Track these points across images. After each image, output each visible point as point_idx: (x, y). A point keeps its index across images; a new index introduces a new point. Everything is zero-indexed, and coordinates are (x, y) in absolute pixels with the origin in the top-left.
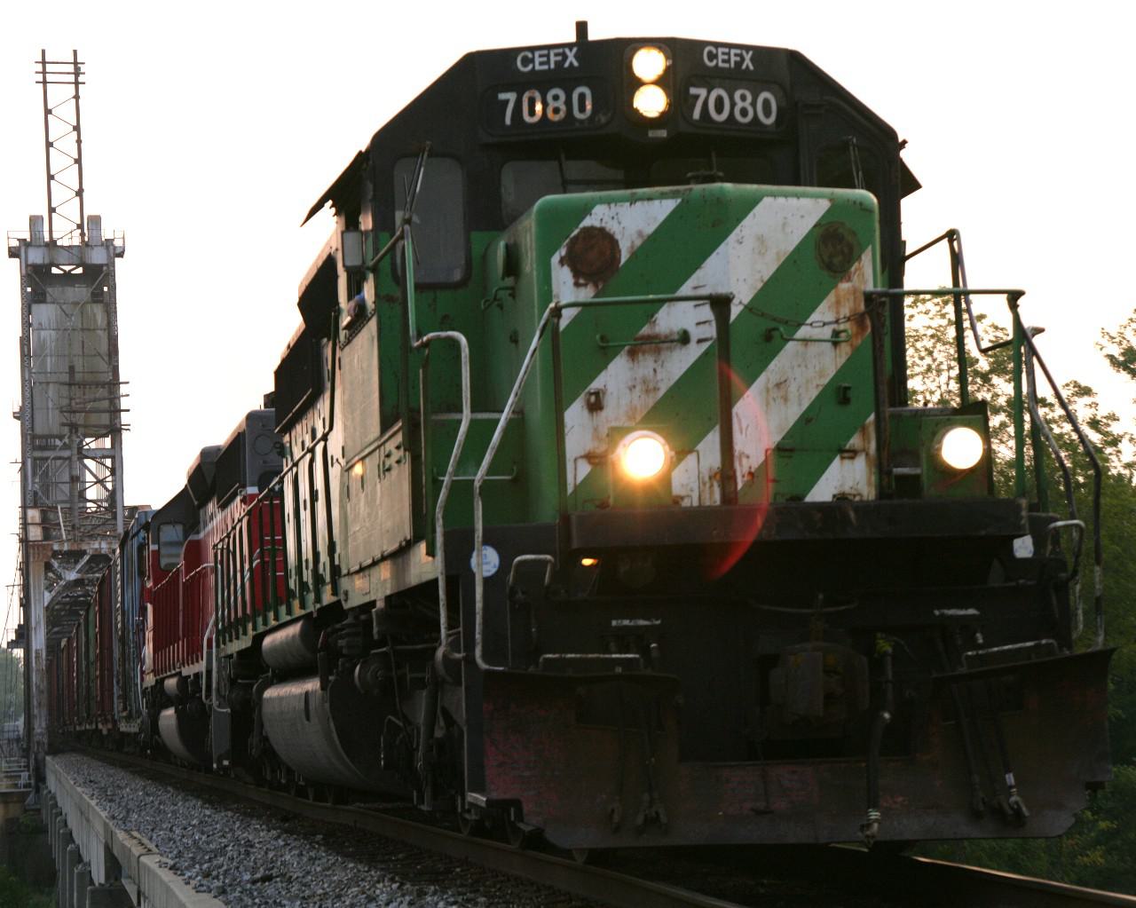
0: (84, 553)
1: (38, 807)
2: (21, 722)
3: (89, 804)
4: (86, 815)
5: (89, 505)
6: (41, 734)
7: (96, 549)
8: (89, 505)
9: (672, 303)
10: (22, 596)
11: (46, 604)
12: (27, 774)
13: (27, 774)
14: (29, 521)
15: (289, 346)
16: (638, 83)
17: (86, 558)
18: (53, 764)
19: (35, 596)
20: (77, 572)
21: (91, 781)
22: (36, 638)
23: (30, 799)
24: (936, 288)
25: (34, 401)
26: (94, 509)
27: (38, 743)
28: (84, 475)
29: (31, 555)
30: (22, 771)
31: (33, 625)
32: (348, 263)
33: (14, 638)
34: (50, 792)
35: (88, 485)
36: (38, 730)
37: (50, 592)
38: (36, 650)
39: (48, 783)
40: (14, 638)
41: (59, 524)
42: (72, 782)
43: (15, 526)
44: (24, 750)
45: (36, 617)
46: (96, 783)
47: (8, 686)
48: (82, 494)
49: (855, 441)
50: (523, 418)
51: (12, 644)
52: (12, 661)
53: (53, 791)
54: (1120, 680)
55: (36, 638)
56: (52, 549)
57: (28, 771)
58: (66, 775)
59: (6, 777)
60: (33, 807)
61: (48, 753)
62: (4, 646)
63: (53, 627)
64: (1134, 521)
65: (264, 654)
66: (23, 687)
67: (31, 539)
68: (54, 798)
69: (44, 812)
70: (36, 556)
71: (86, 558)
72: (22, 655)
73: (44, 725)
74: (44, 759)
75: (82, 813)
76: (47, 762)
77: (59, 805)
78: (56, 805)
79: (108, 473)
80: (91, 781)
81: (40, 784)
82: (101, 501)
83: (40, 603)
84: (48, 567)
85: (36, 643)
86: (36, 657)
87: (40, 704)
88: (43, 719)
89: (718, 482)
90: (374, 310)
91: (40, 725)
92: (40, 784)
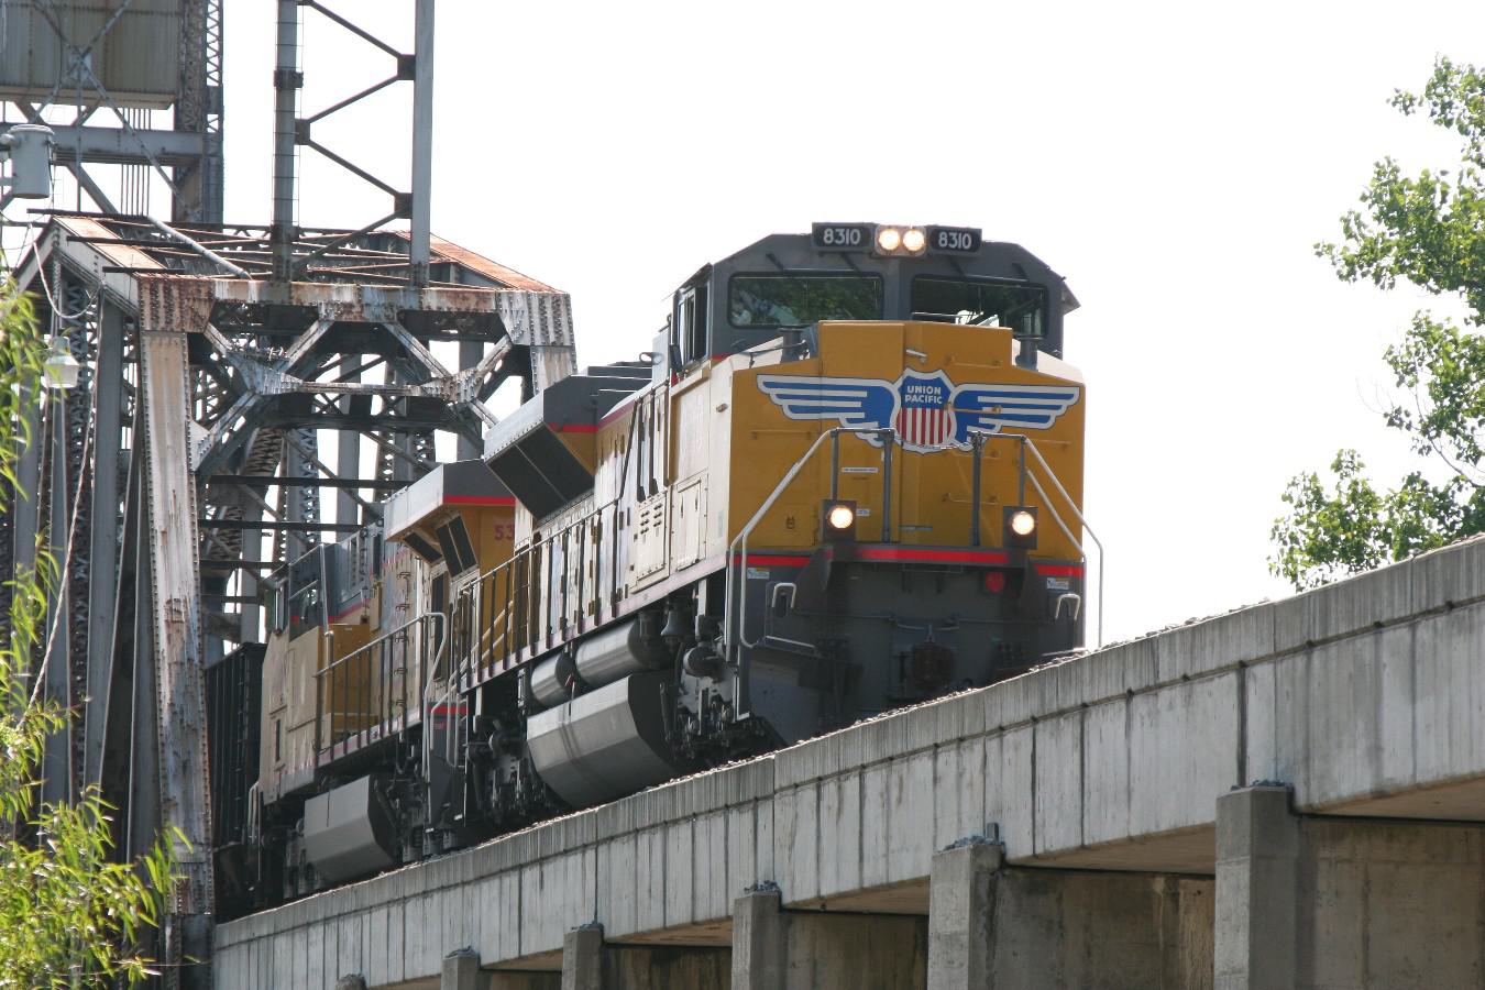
11: (196, 462)
16: (902, 246)
17: (315, 332)
22: (166, 556)
31: (158, 524)
32: (750, 577)
45: (165, 501)
50: (209, 968)
55: (166, 556)
56: (210, 294)
64: (4, 431)
65: (580, 669)
70: (162, 313)
71: (315, 332)
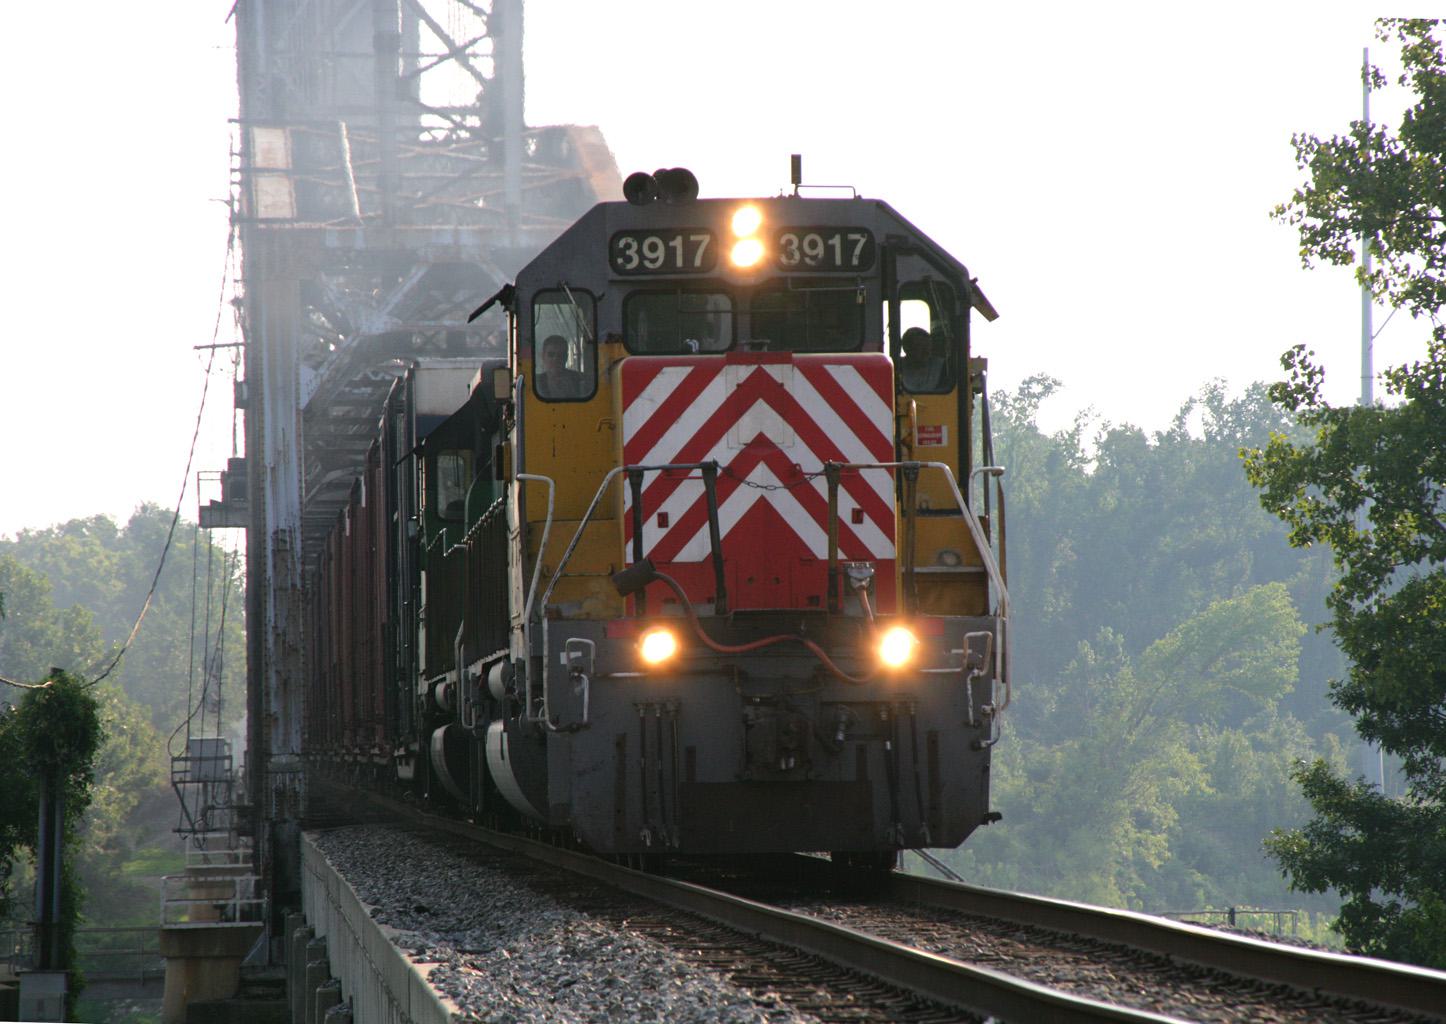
1: (280, 974)
2: (218, 826)
3: (411, 975)
4: (404, 1008)
5: (427, 120)
6: (289, 769)
8: (427, 120)
10: (241, 378)
12: (253, 878)
13: (253, 878)
14: (259, 161)
18: (317, 858)
19: (274, 410)
20: (390, 314)
21: (420, 910)
23: (260, 946)
25: (225, 343)
26: (440, 135)
27: (280, 793)
28: (415, 37)
30: (241, 872)
33: (219, 498)
34: (312, 934)
35: (423, 62)
36: (280, 759)
37: (316, 367)
39: (307, 910)
40: (219, 498)
41: (342, 173)
42: (368, 910)
43: (220, 180)
44: (242, 811)
45: (275, 441)
46: (435, 915)
47: (199, 629)
48: (407, 88)
51: (213, 515)
52: (211, 561)
53: (319, 934)
54: (1051, 938)
55: (275, 493)
57: (255, 871)
58: (352, 888)
59: (197, 886)
60: (262, 975)
61: (307, 825)
62: (190, 516)
63: (327, 470)
66: (244, 633)
67: (262, 213)
68: (321, 951)
69: (293, 988)
72: (242, 549)
73: (296, 743)
74: (297, 842)
75: (391, 1001)
76: (305, 850)
77: (335, 973)
78: (325, 972)
79: (478, 27)
80: (420, 910)
81: (286, 910)
82: (464, 111)
86: (275, 552)
87: (285, 683)
88: (295, 727)
90: (424, 671)
91: (286, 742)
92: (286, 910)
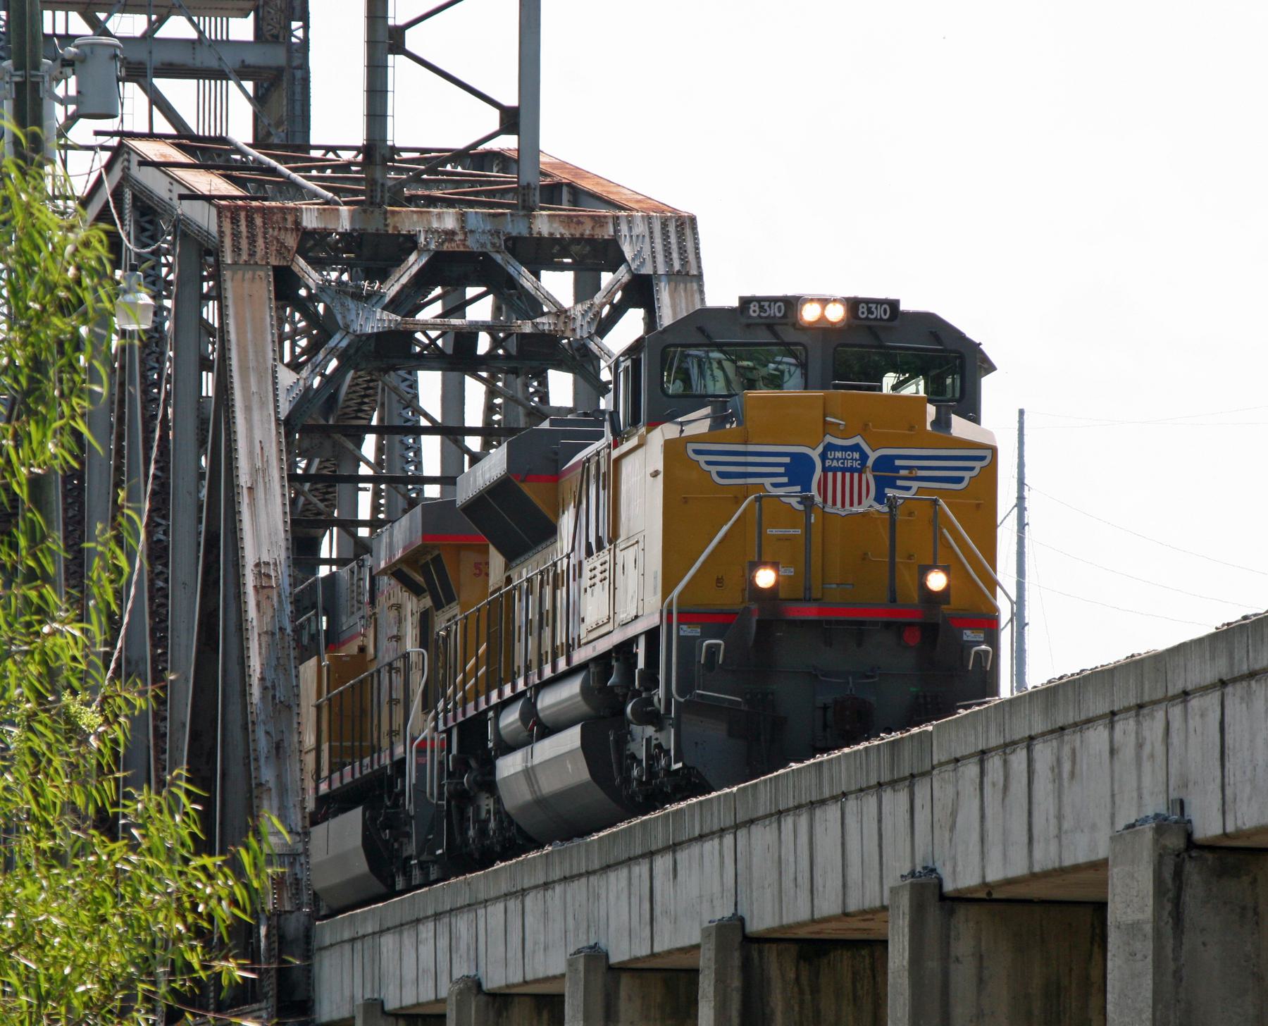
0: (409, 243)
7: (450, 234)
9: (1226, 746)
15: (1133, 656)
22: (254, 515)
24: (1029, 615)
29: (260, 235)
31: (244, 479)
38: (258, 565)
45: (251, 453)
49: (782, 570)
55: (254, 515)
56: (297, 223)
83: (263, 405)
84: (285, 284)
85: (258, 546)
89: (713, 351)
